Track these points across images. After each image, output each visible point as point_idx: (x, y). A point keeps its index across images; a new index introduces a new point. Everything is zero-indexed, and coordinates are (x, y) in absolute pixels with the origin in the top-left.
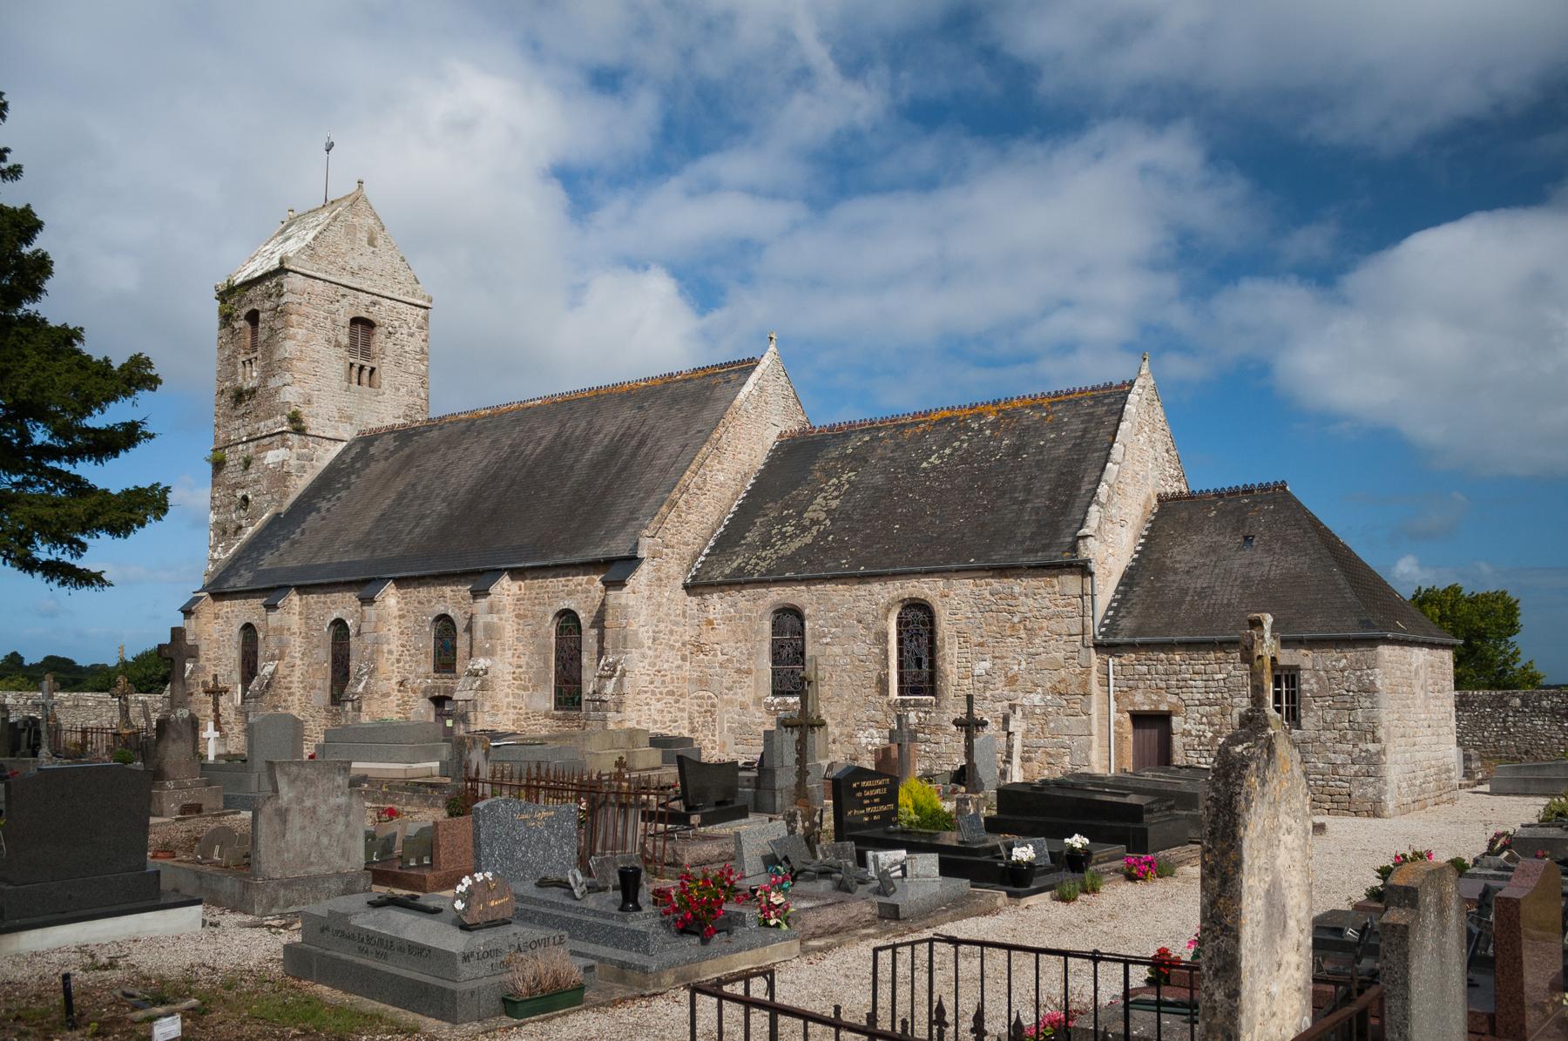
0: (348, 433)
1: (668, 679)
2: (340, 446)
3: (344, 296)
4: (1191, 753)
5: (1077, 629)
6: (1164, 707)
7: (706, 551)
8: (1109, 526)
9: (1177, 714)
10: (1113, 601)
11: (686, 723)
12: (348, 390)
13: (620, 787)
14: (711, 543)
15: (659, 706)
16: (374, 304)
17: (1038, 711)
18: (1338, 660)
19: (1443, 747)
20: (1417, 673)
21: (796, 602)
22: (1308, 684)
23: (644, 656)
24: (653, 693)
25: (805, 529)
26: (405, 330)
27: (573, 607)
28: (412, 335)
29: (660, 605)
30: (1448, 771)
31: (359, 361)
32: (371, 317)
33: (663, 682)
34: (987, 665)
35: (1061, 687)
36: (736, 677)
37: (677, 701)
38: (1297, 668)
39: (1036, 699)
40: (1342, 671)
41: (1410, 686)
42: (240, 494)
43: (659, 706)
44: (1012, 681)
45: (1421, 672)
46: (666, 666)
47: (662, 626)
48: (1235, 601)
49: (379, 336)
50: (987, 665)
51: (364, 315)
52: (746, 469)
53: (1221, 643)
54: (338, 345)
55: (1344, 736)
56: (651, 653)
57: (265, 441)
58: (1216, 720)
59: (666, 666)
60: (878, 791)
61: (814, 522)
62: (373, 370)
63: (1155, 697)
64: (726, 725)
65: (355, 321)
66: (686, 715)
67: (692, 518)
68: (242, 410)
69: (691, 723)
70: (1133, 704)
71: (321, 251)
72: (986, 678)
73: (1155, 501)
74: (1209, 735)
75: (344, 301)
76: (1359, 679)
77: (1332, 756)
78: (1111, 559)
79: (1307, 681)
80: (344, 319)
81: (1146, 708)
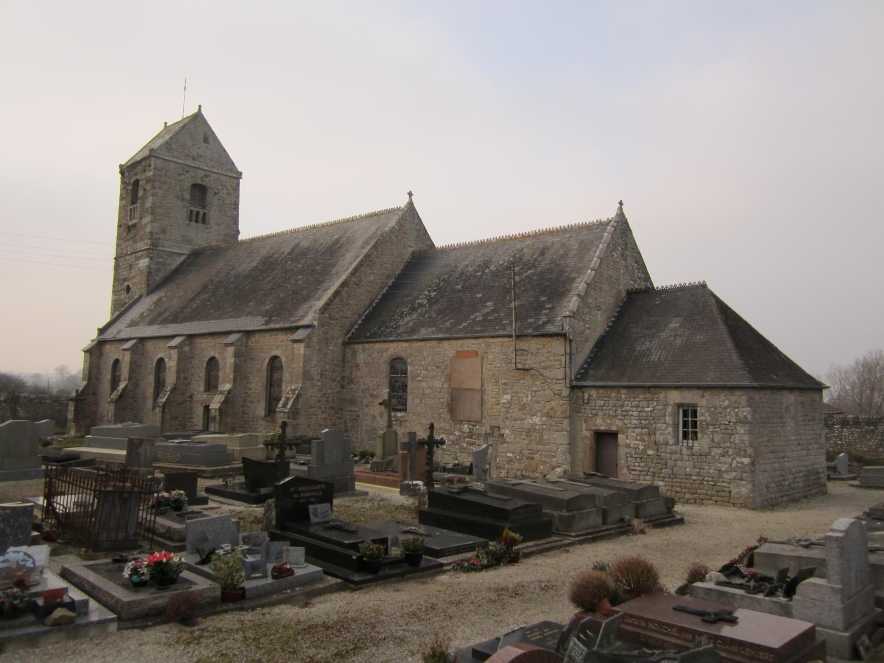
0: (186, 249)
1: (330, 399)
2: (183, 258)
3: (187, 172)
4: (629, 459)
5: (561, 376)
6: (614, 428)
7: (360, 322)
8: (586, 310)
9: (623, 433)
10: (589, 358)
11: (342, 426)
12: (188, 225)
13: (124, 487)
14: (363, 317)
15: (324, 416)
16: (206, 176)
17: (537, 427)
18: (723, 401)
19: (812, 457)
20: (787, 409)
21: (403, 354)
22: (702, 417)
23: (314, 385)
24: (320, 408)
25: (413, 309)
26: (225, 191)
27: (278, 354)
28: (229, 194)
29: (326, 354)
30: (818, 473)
31: (195, 209)
32: (204, 184)
33: (327, 401)
34: (508, 397)
35: (551, 413)
36: (370, 399)
37: (337, 413)
38: (695, 405)
39: (537, 420)
40: (726, 408)
41: (781, 418)
42: (126, 284)
43: (324, 416)
44: (523, 407)
45: (792, 409)
46: (329, 391)
47: (327, 367)
48: (663, 359)
49: (210, 195)
50: (508, 397)
51: (200, 182)
52: (389, 272)
53: (649, 387)
54: (183, 199)
55: (727, 452)
56: (319, 383)
57: (140, 254)
58: (646, 438)
59: (329, 391)
60: (315, 494)
61: (420, 305)
62: (204, 214)
63: (609, 421)
64: (364, 428)
65: (195, 186)
66: (342, 421)
67: (351, 302)
68: (131, 235)
69: (346, 426)
70: (595, 425)
71: (174, 146)
72: (508, 405)
73: (624, 294)
74: (642, 447)
75: (188, 175)
76: (737, 414)
77: (719, 465)
78: (587, 331)
79: (702, 414)
80: (188, 185)
81: (603, 428)
